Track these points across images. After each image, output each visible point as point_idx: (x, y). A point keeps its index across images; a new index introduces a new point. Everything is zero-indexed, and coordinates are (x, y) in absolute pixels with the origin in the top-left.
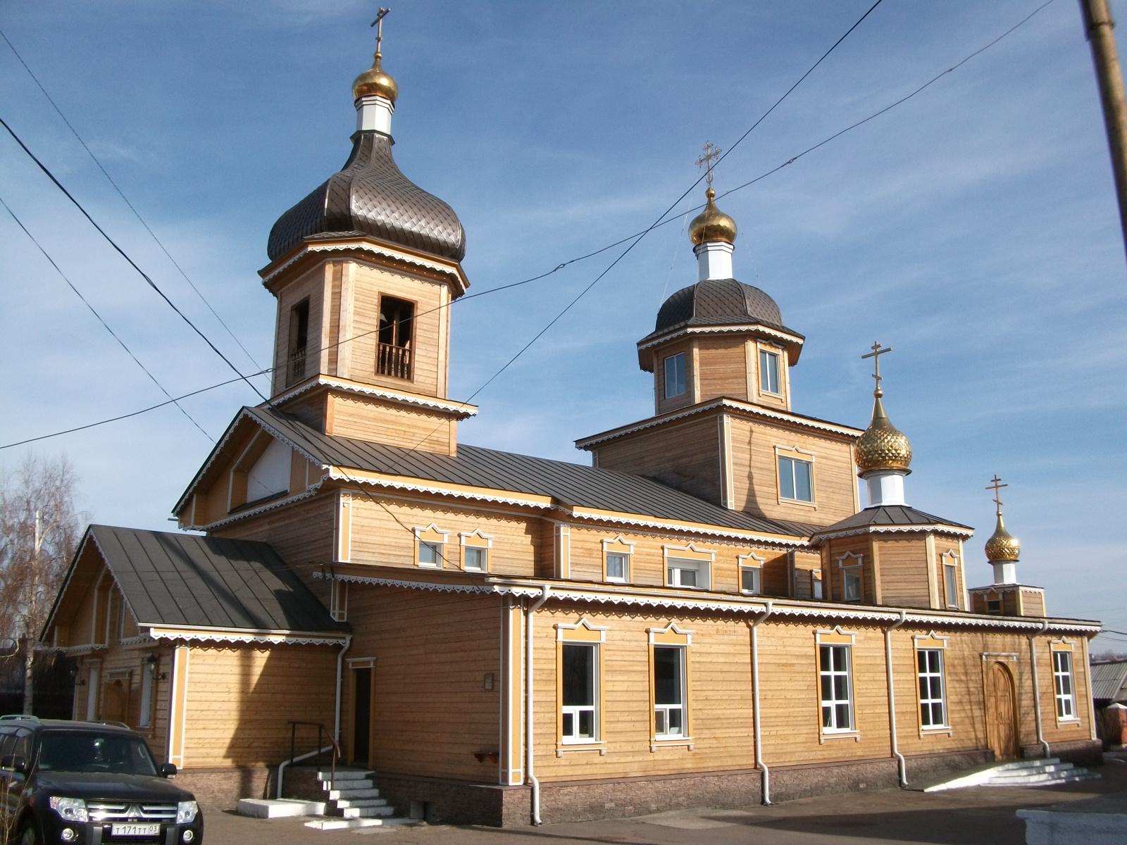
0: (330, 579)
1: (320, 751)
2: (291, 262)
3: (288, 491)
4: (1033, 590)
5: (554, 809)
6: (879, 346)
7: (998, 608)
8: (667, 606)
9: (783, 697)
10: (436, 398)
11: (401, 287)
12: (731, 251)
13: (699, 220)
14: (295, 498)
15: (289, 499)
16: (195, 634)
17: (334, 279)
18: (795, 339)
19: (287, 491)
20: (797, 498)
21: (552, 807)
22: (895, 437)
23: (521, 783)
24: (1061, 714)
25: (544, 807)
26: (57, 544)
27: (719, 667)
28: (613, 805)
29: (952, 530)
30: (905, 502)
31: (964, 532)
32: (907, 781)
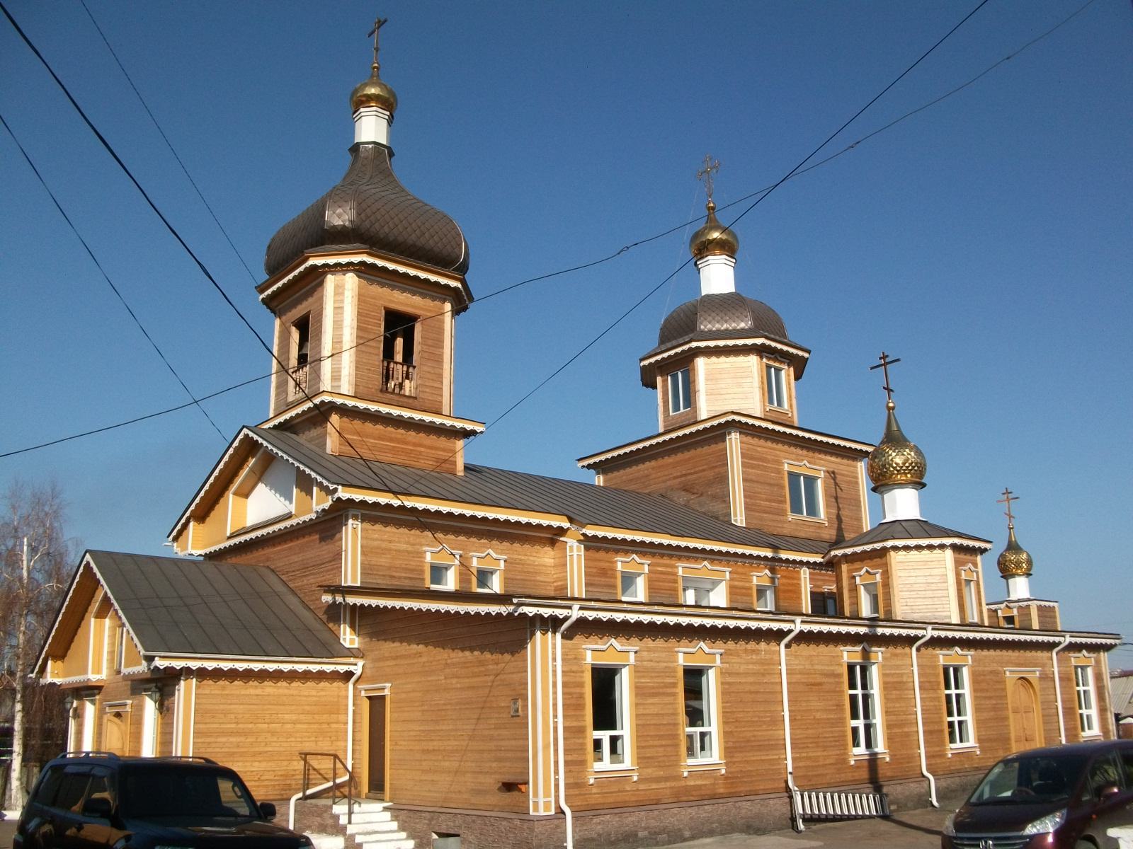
0: (340, 603)
1: (334, 782)
2: (290, 276)
3: (293, 513)
4: (1047, 604)
5: (588, 839)
6: (887, 356)
7: (1013, 623)
8: (720, 627)
9: (812, 717)
10: (442, 415)
11: (404, 301)
12: (733, 265)
13: (696, 236)
14: (300, 520)
15: (293, 522)
16: (186, 662)
17: (336, 294)
18: (800, 353)
19: (291, 512)
20: (807, 514)
21: (585, 837)
22: (897, 451)
23: (553, 812)
24: (1083, 729)
25: (577, 837)
26: (46, 572)
27: (748, 688)
28: (646, 833)
29: (971, 543)
30: (921, 516)
31: (983, 545)
32: (937, 801)
